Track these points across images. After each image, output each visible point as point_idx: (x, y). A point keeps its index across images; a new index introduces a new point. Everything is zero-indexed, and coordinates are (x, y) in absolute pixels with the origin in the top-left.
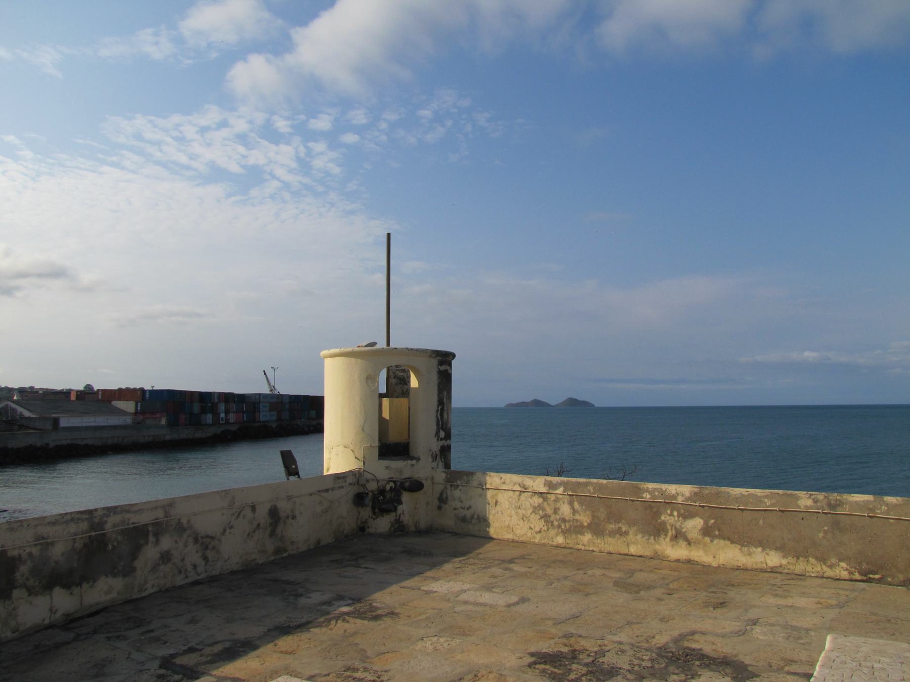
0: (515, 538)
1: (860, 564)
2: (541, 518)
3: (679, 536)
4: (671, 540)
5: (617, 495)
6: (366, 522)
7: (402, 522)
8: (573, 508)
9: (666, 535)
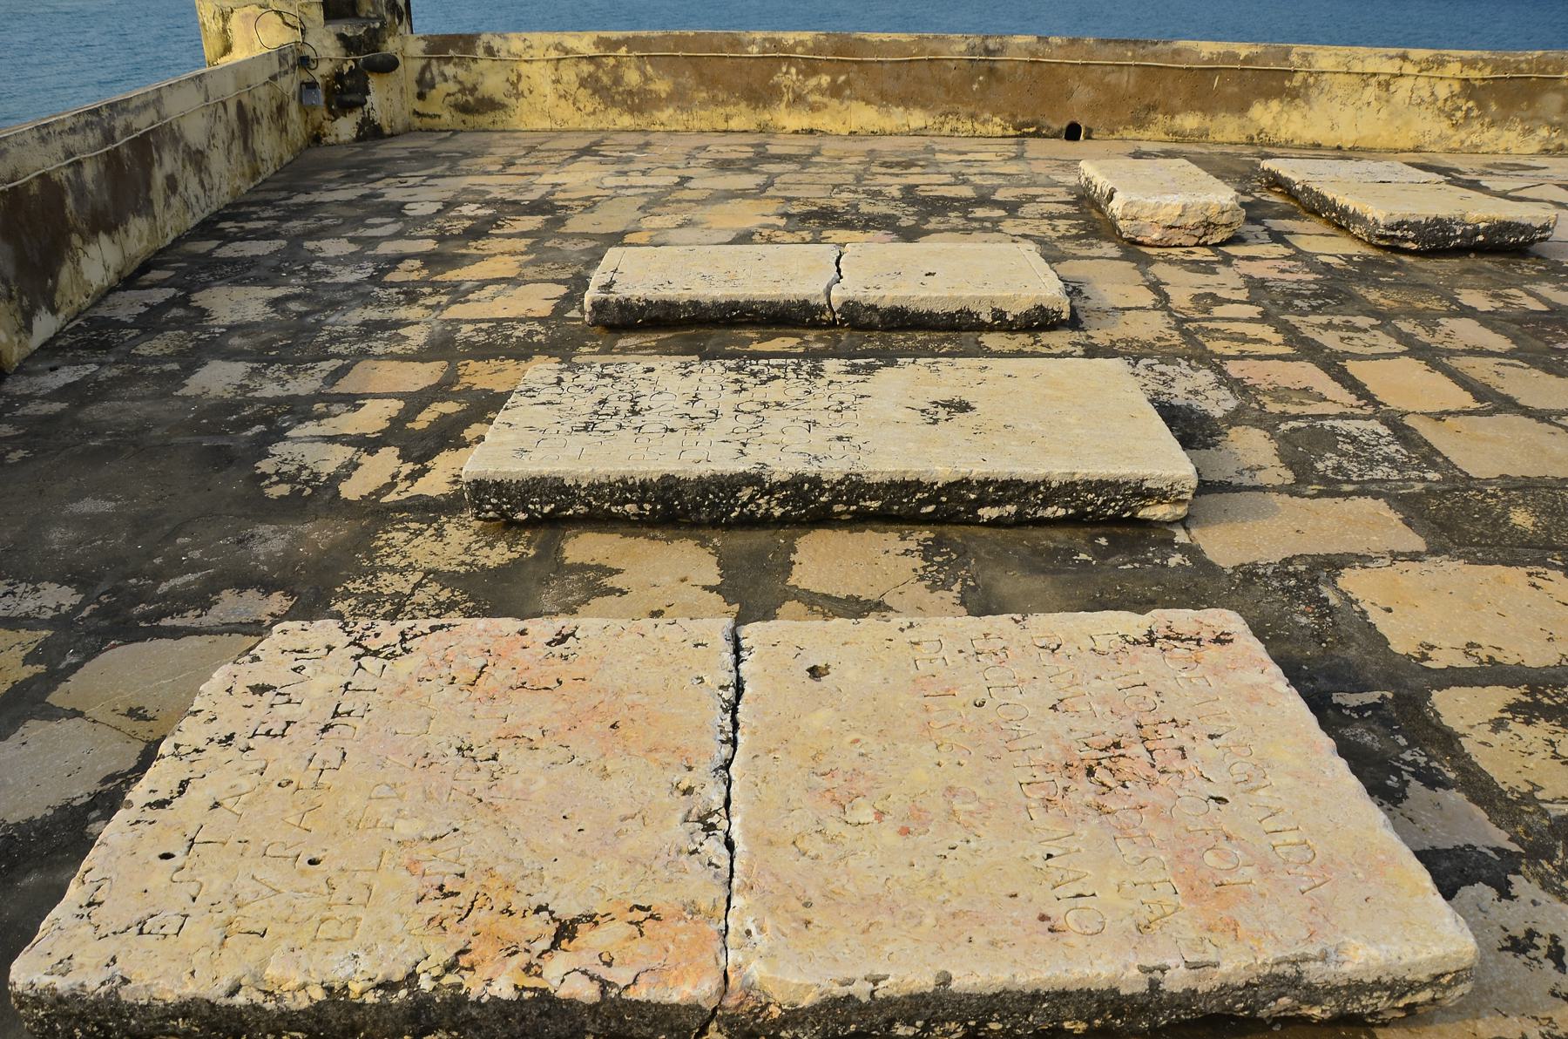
0: (554, 126)
1: (1014, 116)
2: (594, 94)
3: (798, 100)
4: (787, 107)
5: (711, 51)
6: (320, 126)
7: (373, 121)
8: (643, 73)
9: (781, 100)
